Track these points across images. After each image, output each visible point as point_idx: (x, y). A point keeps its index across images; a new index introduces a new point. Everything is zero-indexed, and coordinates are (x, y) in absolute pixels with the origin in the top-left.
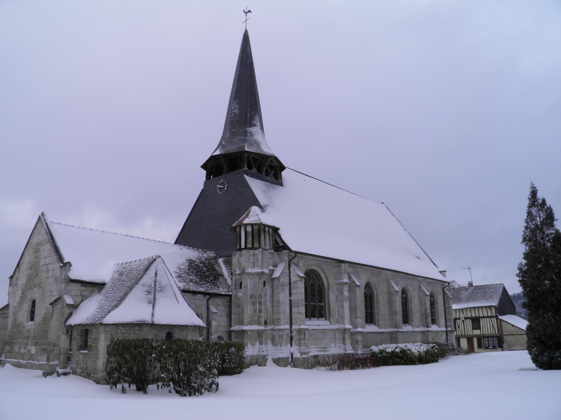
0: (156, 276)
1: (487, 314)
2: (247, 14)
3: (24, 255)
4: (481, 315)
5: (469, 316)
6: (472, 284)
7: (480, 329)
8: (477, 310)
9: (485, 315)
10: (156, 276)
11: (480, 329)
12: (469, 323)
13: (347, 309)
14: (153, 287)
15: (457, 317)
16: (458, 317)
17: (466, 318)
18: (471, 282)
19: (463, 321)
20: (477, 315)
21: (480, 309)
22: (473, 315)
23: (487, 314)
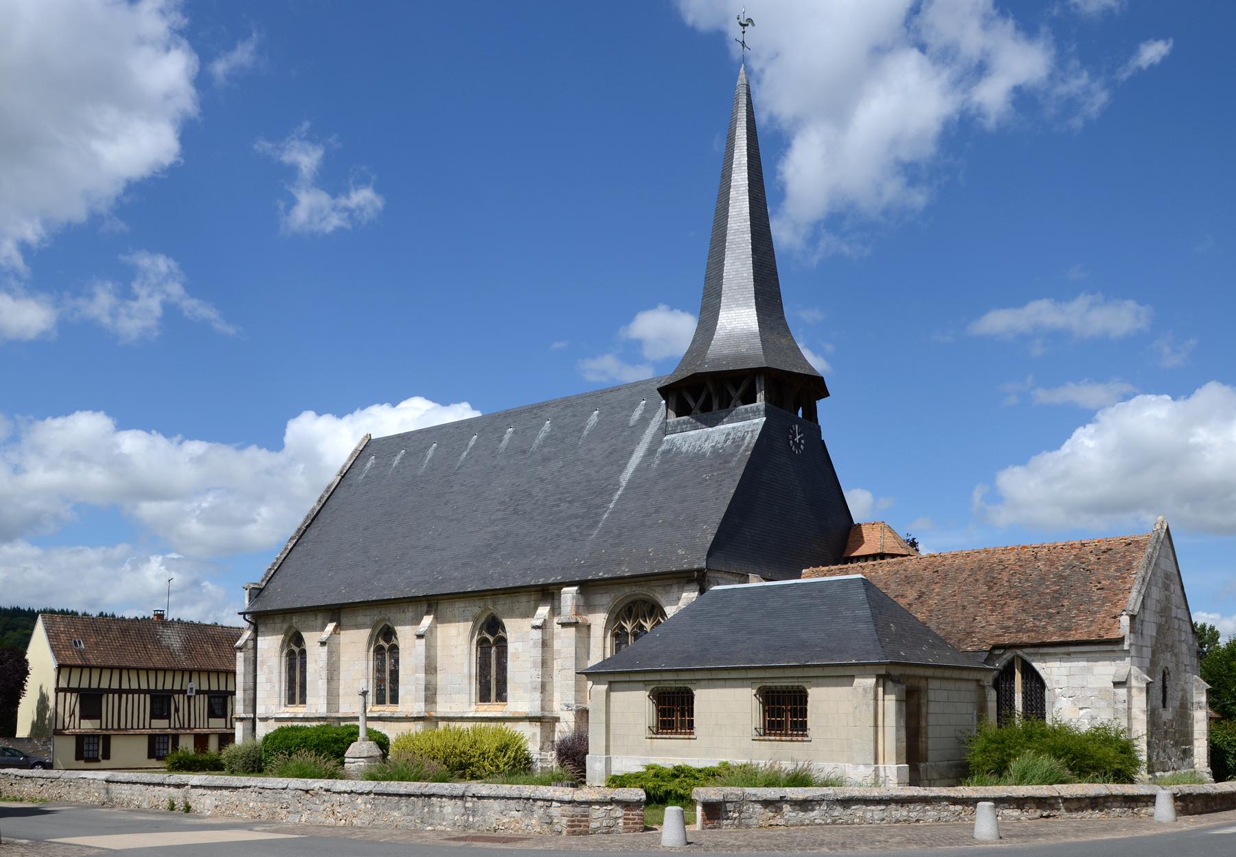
0: (243, 787)
1: (173, 686)
2: (911, 59)
3: (785, 669)
4: (104, 685)
5: (205, 687)
6: (163, 615)
7: (168, 717)
8: (86, 673)
9: (134, 686)
10: (243, 787)
11: (168, 717)
12: (202, 703)
13: (972, 704)
14: (447, 723)
15: (63, 694)
16: (177, 687)
17: (199, 692)
18: (161, 611)
19: (189, 698)
20: (223, 688)
21: (104, 671)
22: (214, 687)
23: (173, 686)
